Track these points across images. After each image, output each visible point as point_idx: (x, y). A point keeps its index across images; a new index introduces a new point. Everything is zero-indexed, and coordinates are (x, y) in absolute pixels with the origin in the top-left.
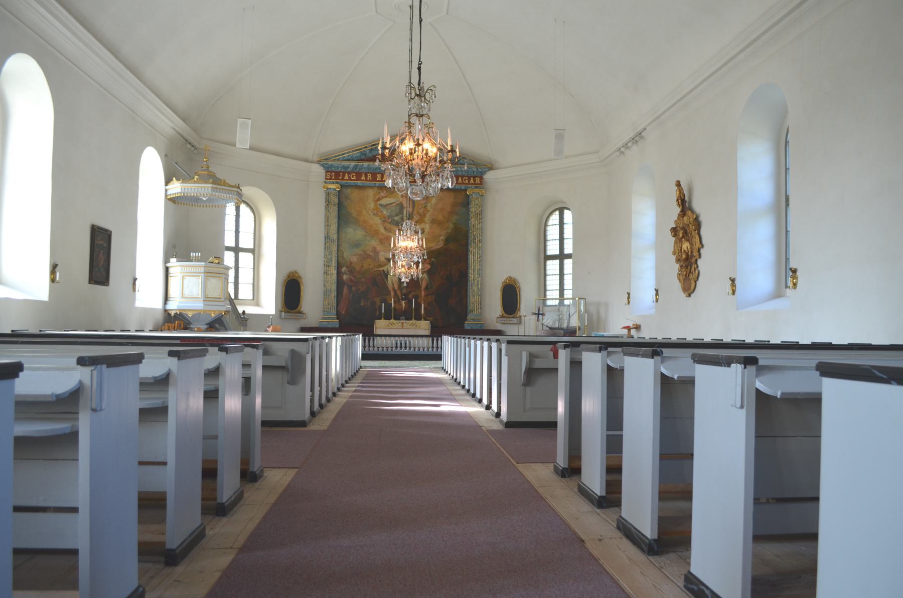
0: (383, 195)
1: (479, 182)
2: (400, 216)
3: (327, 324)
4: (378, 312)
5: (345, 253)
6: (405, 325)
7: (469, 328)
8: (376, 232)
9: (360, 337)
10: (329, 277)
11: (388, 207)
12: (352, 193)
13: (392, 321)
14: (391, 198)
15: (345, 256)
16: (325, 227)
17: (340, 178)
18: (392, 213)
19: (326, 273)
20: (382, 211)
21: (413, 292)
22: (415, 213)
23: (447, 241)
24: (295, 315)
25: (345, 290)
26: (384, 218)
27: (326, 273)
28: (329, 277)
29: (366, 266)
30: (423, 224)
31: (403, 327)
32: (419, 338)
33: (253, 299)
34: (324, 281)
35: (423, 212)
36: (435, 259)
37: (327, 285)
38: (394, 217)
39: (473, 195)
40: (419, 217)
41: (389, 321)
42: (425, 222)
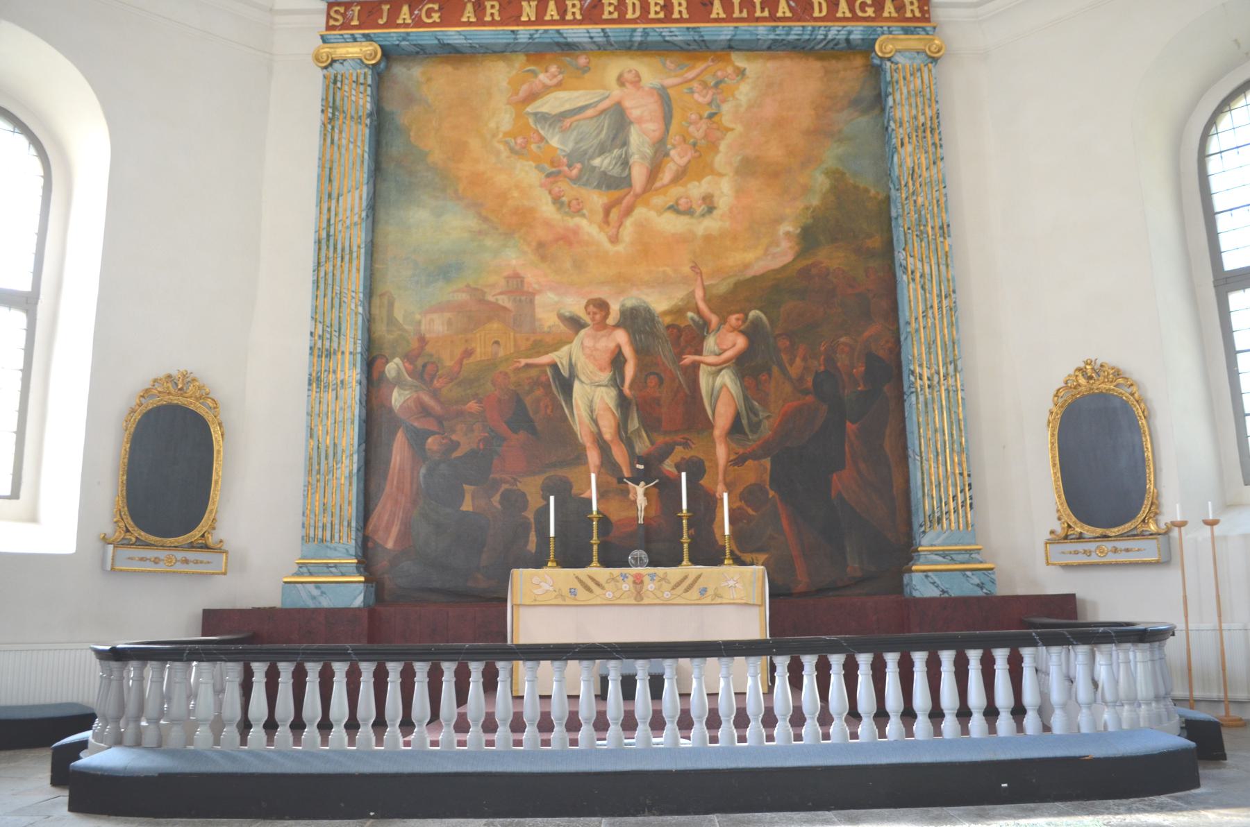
0: (547, 82)
1: (918, 14)
2: (616, 152)
3: (316, 592)
4: (533, 537)
5: (397, 305)
6: (650, 586)
7: (931, 592)
8: (523, 219)
9: (1084, 730)
10: (331, 395)
11: (567, 122)
12: (429, 80)
13: (595, 571)
14: (576, 89)
15: (399, 315)
16: (320, 201)
17: (381, 22)
18: (584, 146)
19: (318, 379)
20: (542, 139)
21: (679, 449)
22: (674, 138)
23: (808, 238)
24: (169, 558)
25: (399, 452)
26: (553, 163)
27: (315, 381)
28: (331, 395)
29: (482, 351)
30: (708, 178)
31: (639, 595)
32: (545, 664)
33: (15, 494)
34: (310, 414)
35: (706, 136)
36: (760, 309)
37: (320, 431)
38: (592, 158)
39: (898, 58)
40: (690, 154)
41: (578, 571)
42: (713, 172)
